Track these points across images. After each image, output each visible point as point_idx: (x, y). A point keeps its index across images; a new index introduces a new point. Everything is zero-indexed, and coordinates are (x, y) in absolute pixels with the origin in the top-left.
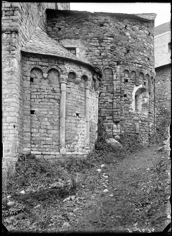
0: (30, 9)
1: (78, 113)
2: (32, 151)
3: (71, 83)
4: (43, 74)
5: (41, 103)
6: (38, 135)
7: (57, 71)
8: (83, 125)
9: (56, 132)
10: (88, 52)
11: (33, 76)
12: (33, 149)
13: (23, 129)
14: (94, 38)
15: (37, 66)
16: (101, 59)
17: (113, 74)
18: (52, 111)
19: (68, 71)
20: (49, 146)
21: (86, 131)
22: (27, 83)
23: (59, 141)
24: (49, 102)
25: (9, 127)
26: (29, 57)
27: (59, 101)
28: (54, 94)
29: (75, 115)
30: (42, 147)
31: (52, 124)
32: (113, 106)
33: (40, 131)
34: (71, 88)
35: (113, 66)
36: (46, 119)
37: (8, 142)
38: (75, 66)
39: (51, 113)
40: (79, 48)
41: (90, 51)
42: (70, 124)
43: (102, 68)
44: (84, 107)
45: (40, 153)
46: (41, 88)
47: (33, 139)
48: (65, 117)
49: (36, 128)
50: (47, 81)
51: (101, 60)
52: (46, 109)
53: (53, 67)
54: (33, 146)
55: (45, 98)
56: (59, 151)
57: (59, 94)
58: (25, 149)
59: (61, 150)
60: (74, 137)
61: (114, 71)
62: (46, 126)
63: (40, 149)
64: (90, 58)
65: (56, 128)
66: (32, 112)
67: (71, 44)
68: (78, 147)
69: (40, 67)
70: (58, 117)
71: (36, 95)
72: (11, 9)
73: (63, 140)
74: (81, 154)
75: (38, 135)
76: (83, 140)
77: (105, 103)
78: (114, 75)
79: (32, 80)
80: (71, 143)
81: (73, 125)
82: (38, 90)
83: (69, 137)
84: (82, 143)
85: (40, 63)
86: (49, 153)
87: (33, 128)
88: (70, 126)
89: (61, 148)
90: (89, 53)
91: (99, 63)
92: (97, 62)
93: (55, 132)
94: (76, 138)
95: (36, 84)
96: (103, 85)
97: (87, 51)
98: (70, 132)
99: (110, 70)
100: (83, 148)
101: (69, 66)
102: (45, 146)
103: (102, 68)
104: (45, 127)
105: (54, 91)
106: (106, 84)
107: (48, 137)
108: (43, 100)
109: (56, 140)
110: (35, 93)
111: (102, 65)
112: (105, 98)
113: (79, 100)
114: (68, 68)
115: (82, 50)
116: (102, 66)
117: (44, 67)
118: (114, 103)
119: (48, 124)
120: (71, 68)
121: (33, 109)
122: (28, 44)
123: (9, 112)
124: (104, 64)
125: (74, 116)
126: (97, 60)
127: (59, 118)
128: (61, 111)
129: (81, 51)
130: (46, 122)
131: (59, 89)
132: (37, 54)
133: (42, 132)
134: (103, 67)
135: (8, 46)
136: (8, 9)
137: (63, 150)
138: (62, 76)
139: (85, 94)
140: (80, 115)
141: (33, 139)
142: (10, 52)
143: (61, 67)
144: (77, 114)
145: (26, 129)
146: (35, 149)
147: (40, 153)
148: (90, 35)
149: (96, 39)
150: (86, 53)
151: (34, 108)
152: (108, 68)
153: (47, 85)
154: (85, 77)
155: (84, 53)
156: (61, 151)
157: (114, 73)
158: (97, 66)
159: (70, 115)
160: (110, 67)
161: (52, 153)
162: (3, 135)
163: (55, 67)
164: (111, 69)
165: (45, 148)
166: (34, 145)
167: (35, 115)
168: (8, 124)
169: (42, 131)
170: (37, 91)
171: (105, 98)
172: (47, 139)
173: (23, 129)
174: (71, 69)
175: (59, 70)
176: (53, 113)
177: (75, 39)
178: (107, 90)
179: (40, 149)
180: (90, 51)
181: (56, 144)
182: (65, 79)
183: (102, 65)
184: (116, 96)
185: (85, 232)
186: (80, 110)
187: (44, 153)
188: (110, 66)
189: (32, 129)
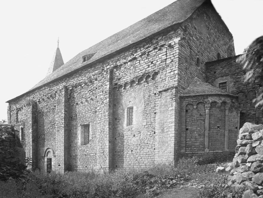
1: (218, 126)
2: (186, 151)
4: (193, 107)
6: (190, 142)
9: (202, 140)
11: (188, 109)
12: (187, 151)
13: (181, 140)
14: (241, 72)
15: (190, 103)
16: (247, 85)
19: (210, 102)
20: (197, 148)
22: (184, 113)
24: (198, 122)
25: (171, 140)
26: (185, 99)
27: (204, 121)
29: (217, 127)
30: (193, 149)
31: (199, 135)
32: (256, 116)
33: (191, 140)
34: (213, 112)
36: (196, 132)
38: (216, 98)
39: (199, 128)
41: (237, 82)
43: (246, 92)
44: (224, 122)
50: (197, 110)
51: (246, 86)
52: (195, 127)
53: (200, 101)
55: (195, 120)
56: (204, 151)
57: (204, 116)
58: (182, 151)
61: (256, 91)
62: (195, 136)
63: (192, 151)
64: (237, 86)
65: (202, 137)
66: (187, 129)
67: (223, 80)
69: (191, 103)
70: (204, 130)
71: (189, 119)
75: (190, 142)
78: (257, 94)
81: (215, 134)
82: (191, 116)
85: (192, 101)
86: (197, 152)
91: (245, 88)
92: (242, 88)
93: (202, 139)
96: (247, 103)
98: (212, 138)
99: (254, 91)
101: (212, 98)
102: (195, 148)
105: (201, 115)
107: (197, 143)
108: (194, 121)
109: (202, 144)
110: (189, 118)
111: (247, 89)
112: (249, 111)
117: (194, 103)
119: (197, 135)
120: (213, 100)
121: (187, 128)
123: (171, 131)
126: (243, 87)
127: (205, 131)
130: (196, 134)
132: (189, 96)
133: (193, 140)
134: (247, 91)
136: (172, 76)
138: (206, 106)
139: (225, 113)
140: (220, 127)
144: (218, 127)
145: (183, 139)
147: (191, 152)
149: (242, 72)
150: (234, 84)
151: (188, 127)
152: (252, 91)
153: (196, 112)
155: (233, 84)
156: (205, 150)
157: (257, 93)
160: (253, 90)
161: (199, 152)
162: (63, 152)
163: (202, 101)
165: (195, 149)
168: (170, 138)
169: (193, 140)
170: (190, 117)
171: (249, 111)
172: (196, 144)
173: (181, 140)
174: (213, 100)
175: (205, 102)
179: (192, 151)
180: (237, 82)
181: (202, 147)
182: (208, 107)
183: (247, 89)
186: (220, 124)
187: (193, 152)
188: (253, 89)
189: (187, 139)
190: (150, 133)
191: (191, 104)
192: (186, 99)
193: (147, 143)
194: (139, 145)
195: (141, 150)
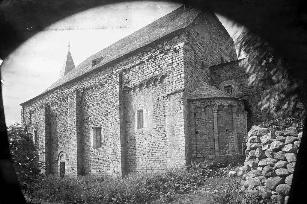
0: (194, 73)
3: (221, 111)
5: (201, 126)
6: (201, 146)
7: (210, 106)
8: (232, 137)
10: (240, 86)
11: (196, 112)
15: (197, 106)
17: (260, 97)
18: (208, 130)
20: (208, 152)
21: (235, 140)
22: (192, 116)
23: (215, 148)
25: (182, 143)
27: (213, 124)
28: (210, 120)
29: (226, 131)
30: (204, 152)
31: (209, 138)
35: (260, 92)
36: (205, 136)
37: (182, 151)
38: (222, 101)
39: (208, 132)
40: (233, 85)
41: (242, 85)
42: (222, 137)
43: (251, 95)
44: (232, 125)
45: (202, 156)
46: (201, 118)
47: (198, 148)
48: (217, 133)
49: (199, 142)
51: (250, 89)
53: (207, 104)
54: (198, 152)
56: (215, 155)
58: (193, 155)
59: (216, 154)
60: (226, 145)
63: (202, 154)
64: (242, 89)
65: (212, 140)
66: (197, 133)
67: (228, 83)
68: (229, 151)
69: (199, 106)
70: (213, 133)
71: (198, 122)
72: (180, 79)
73: (217, 147)
74: (232, 155)
75: (201, 146)
76: (233, 146)
77: (256, 118)
79: (195, 114)
80: (223, 149)
82: (199, 119)
83: (222, 145)
84: (232, 148)
85: (199, 104)
86: (208, 156)
87: (197, 141)
88: (222, 138)
89: (216, 152)
90: (241, 86)
92: (247, 91)
94: (227, 145)
95: (198, 116)
97: (239, 86)
98: (222, 142)
100: (234, 151)
102: (205, 152)
103: (251, 95)
104: (205, 140)
105: (209, 118)
106: (255, 105)
109: (212, 148)
110: (198, 121)
112: (255, 115)
113: (228, 121)
114: (217, 103)
115: (235, 86)
116: (251, 93)
117: (201, 106)
118: (263, 117)
119: (207, 138)
122: (193, 94)
123: (181, 134)
124: (253, 91)
125: (225, 132)
128: (215, 130)
129: (235, 86)
130: (205, 137)
131: (212, 117)
135: (179, 99)
136: (179, 79)
137: (217, 154)
139: (232, 116)
140: (229, 131)
141: (198, 148)
142: (181, 102)
143: (213, 103)
144: (227, 130)
146: (200, 154)
148: (241, 75)
150: (239, 87)
154: (231, 106)
158: (247, 94)
159: (222, 131)
161: (210, 156)
163: (209, 104)
164: (259, 94)
165: (205, 153)
166: (199, 152)
167: (198, 134)
168: (181, 141)
169: (203, 143)
170: (199, 120)
171: (255, 115)
172: (206, 147)
174: (220, 103)
176: (210, 131)
177: (230, 80)
178: (257, 109)
179: (202, 154)
180: (242, 85)
181: (213, 150)
184: (264, 112)
185: (55, 121)
188: (257, 92)
190: (160, 137)
191: (199, 107)
192: (194, 102)
193: (159, 147)
194: (151, 149)
195: (152, 153)
